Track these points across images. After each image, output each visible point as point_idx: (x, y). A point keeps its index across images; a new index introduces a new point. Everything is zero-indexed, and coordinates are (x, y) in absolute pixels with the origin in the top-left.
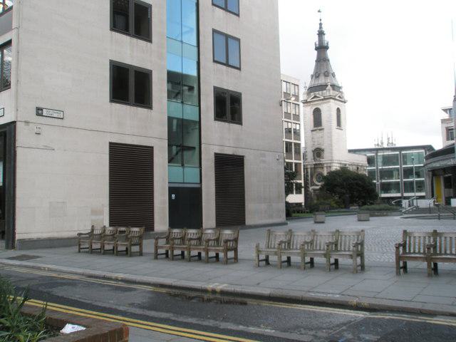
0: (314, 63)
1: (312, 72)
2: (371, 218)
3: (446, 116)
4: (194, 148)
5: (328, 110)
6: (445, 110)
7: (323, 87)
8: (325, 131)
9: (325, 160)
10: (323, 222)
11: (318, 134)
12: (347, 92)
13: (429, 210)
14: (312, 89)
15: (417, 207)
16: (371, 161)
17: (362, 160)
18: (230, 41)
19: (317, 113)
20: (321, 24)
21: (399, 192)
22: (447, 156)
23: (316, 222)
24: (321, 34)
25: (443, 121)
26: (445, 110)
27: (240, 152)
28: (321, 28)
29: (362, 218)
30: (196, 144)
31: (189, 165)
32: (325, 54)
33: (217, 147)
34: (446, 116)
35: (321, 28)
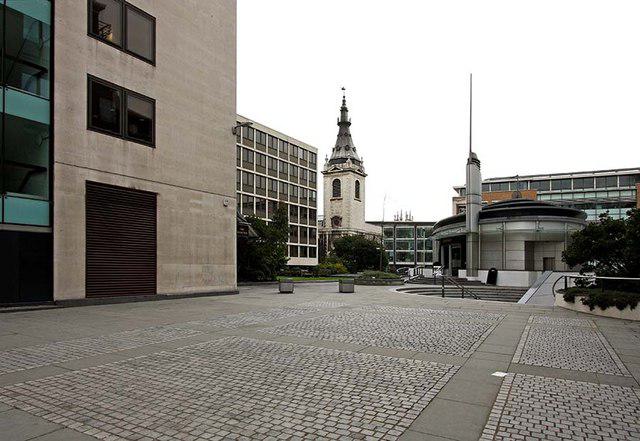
0: (336, 138)
1: (334, 145)
2: (357, 288)
3: (457, 195)
4: (45, 169)
5: (347, 182)
6: (457, 189)
7: (343, 160)
8: (344, 201)
9: (343, 227)
10: (291, 292)
11: (336, 204)
12: (367, 168)
13: (434, 280)
14: (333, 161)
15: (422, 276)
16: (388, 233)
17: (378, 230)
18: (130, 14)
19: (337, 184)
20: (344, 101)
21: (412, 261)
22: (456, 225)
23: (282, 292)
24: (344, 110)
25: (454, 199)
26: (457, 189)
27: (149, 187)
28: (344, 104)
29: (344, 289)
30: (47, 166)
31: (12, 194)
32: (348, 130)
33: (95, 173)
34: (457, 195)
35: (344, 104)
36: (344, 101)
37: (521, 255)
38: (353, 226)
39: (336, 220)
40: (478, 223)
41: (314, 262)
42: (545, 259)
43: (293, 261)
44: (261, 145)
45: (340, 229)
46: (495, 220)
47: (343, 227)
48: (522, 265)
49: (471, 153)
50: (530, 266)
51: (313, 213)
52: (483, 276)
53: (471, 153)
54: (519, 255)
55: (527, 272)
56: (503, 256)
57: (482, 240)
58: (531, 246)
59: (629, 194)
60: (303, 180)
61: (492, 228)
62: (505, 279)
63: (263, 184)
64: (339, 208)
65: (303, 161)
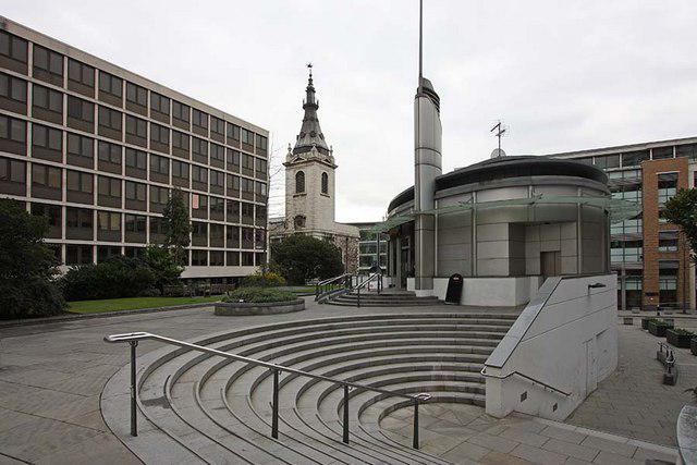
5: (313, 174)
7: (307, 148)
11: (300, 200)
12: (338, 158)
14: (298, 150)
19: (300, 177)
20: (310, 80)
24: (310, 90)
36: (310, 80)
37: (503, 250)
38: (316, 228)
39: (300, 220)
40: (435, 199)
41: (252, 271)
42: (543, 254)
43: (189, 272)
44: (217, 134)
45: (304, 230)
46: (456, 190)
47: (307, 229)
48: (505, 267)
49: (422, 80)
50: (518, 269)
51: (263, 211)
52: (441, 288)
53: (422, 80)
54: (498, 247)
55: (514, 279)
56: (473, 253)
57: (441, 226)
58: (520, 232)
59: (634, 174)
60: (248, 169)
61: (454, 205)
62: (477, 292)
63: (215, 179)
64: (303, 206)
65: (248, 146)
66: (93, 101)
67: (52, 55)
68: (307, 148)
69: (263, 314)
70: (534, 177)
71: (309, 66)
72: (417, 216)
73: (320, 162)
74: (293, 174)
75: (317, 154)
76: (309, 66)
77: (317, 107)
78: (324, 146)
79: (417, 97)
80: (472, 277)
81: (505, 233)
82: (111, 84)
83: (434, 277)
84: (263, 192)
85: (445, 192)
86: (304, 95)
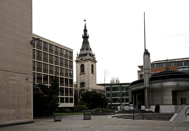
5: (87, 65)
7: (85, 55)
11: (82, 76)
12: (97, 58)
19: (82, 66)
20: (85, 26)
24: (85, 31)
36: (85, 26)
37: (171, 98)
38: (90, 87)
39: (83, 84)
41: (72, 105)
43: (61, 105)
45: (84, 88)
46: (157, 81)
48: (171, 102)
50: (175, 103)
51: (71, 81)
52: (153, 108)
54: (169, 97)
57: (152, 91)
58: (175, 93)
62: (164, 109)
64: (84, 78)
65: (66, 56)
66: (47, 53)
67: (46, 43)
68: (85, 55)
69: (107, 115)
70: (178, 79)
71: (85, 21)
72: (145, 88)
73: (91, 60)
74: (79, 65)
75: (89, 57)
76: (85, 21)
77: (88, 37)
78: (91, 53)
79: (144, 55)
80: (162, 105)
81: (171, 93)
82: (45, 44)
83: (150, 105)
84: (71, 73)
85: (153, 81)
86: (83, 33)
